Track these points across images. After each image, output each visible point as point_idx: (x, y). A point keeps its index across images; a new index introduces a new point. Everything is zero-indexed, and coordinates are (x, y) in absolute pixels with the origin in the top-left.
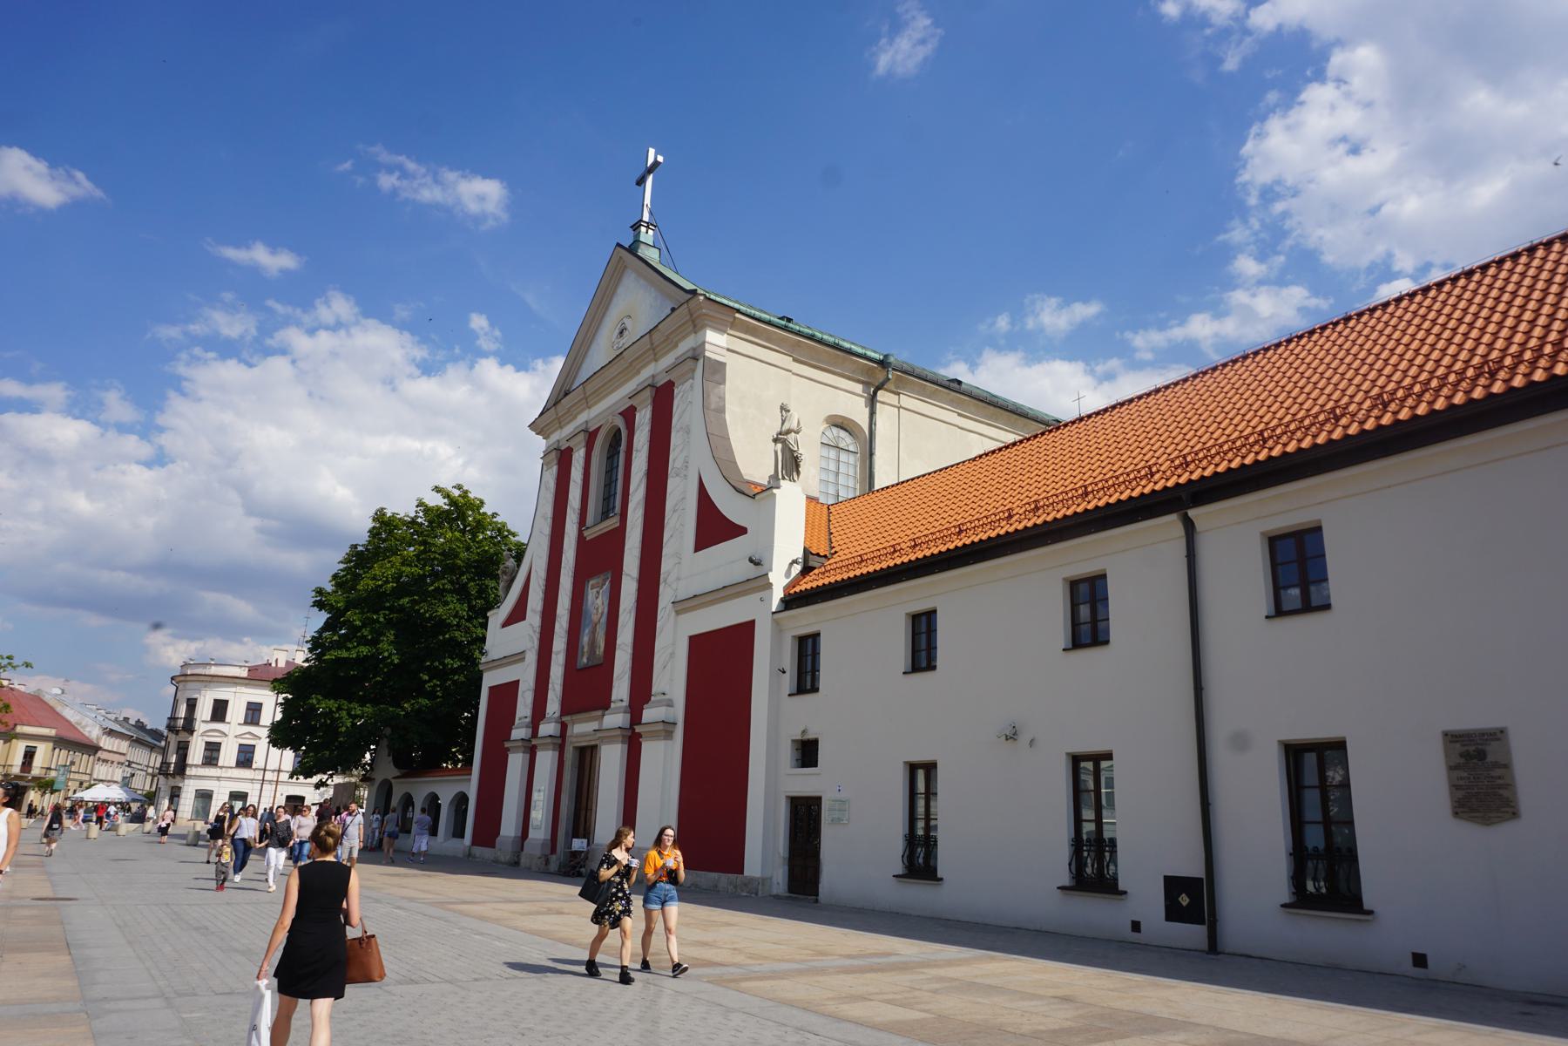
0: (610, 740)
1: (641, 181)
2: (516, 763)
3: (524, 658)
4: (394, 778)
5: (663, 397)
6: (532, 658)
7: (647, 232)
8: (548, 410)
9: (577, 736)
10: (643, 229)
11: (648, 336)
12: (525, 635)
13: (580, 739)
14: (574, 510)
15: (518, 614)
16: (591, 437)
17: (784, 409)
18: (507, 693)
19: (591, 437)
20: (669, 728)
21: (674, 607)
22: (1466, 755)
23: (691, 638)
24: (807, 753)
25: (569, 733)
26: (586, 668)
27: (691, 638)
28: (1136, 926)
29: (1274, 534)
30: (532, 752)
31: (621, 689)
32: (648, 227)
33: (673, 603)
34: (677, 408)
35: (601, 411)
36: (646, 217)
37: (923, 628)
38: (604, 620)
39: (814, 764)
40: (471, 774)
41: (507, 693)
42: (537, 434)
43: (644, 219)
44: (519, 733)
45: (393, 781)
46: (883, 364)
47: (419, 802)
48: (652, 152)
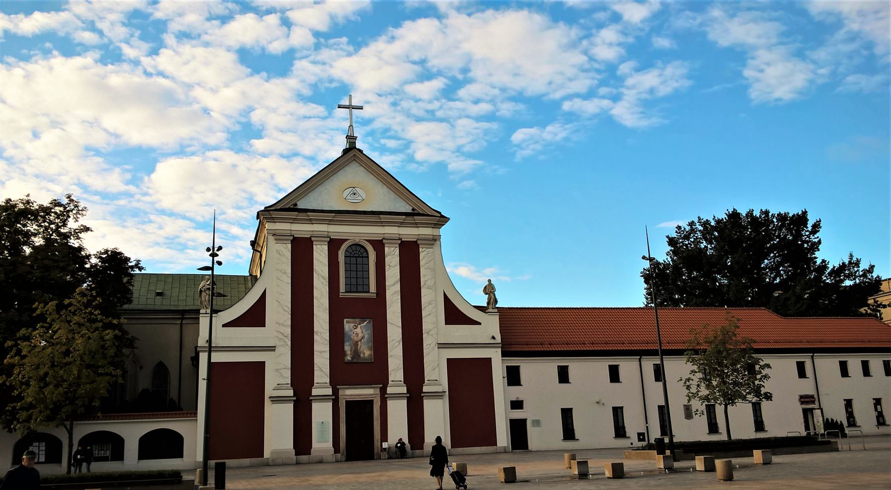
3: (275, 350)
14: (323, 277)
22: (687, 408)
23: (842, 377)
25: (341, 392)
26: (349, 363)
27: (842, 377)
28: (632, 444)
34: (424, 257)
39: (563, 410)
40: (197, 417)
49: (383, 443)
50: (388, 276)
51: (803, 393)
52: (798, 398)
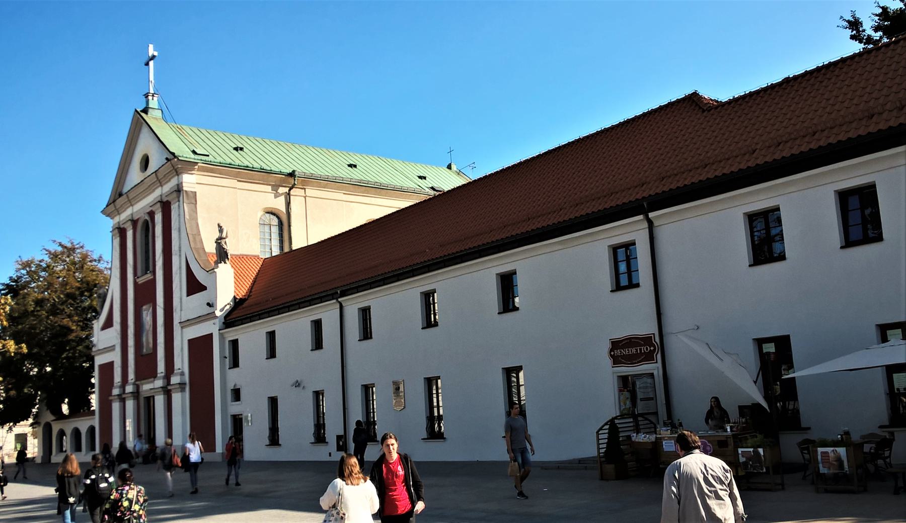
0: (158, 393)
1: (147, 64)
2: (116, 407)
4: (52, 421)
5: (166, 206)
6: (118, 349)
7: (153, 99)
8: (110, 204)
9: (147, 391)
10: (150, 98)
11: (154, 174)
12: (112, 336)
13: (147, 393)
15: (108, 324)
16: (134, 222)
17: (219, 226)
18: (108, 368)
19: (134, 222)
20: (183, 386)
21: (180, 325)
24: (237, 394)
29: (502, 274)
30: (123, 401)
31: (161, 367)
32: (153, 96)
33: (180, 323)
35: (140, 208)
36: (152, 91)
37: (507, 283)
38: (151, 329)
41: (108, 368)
42: (106, 216)
43: (151, 92)
44: (116, 391)
45: (52, 423)
46: (292, 175)
47: (68, 432)
48: (151, 47)
49: (899, 331)
50: (174, 246)
51: (621, 334)
52: (608, 346)
